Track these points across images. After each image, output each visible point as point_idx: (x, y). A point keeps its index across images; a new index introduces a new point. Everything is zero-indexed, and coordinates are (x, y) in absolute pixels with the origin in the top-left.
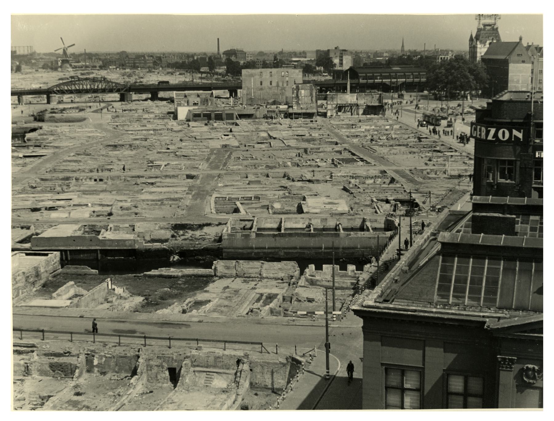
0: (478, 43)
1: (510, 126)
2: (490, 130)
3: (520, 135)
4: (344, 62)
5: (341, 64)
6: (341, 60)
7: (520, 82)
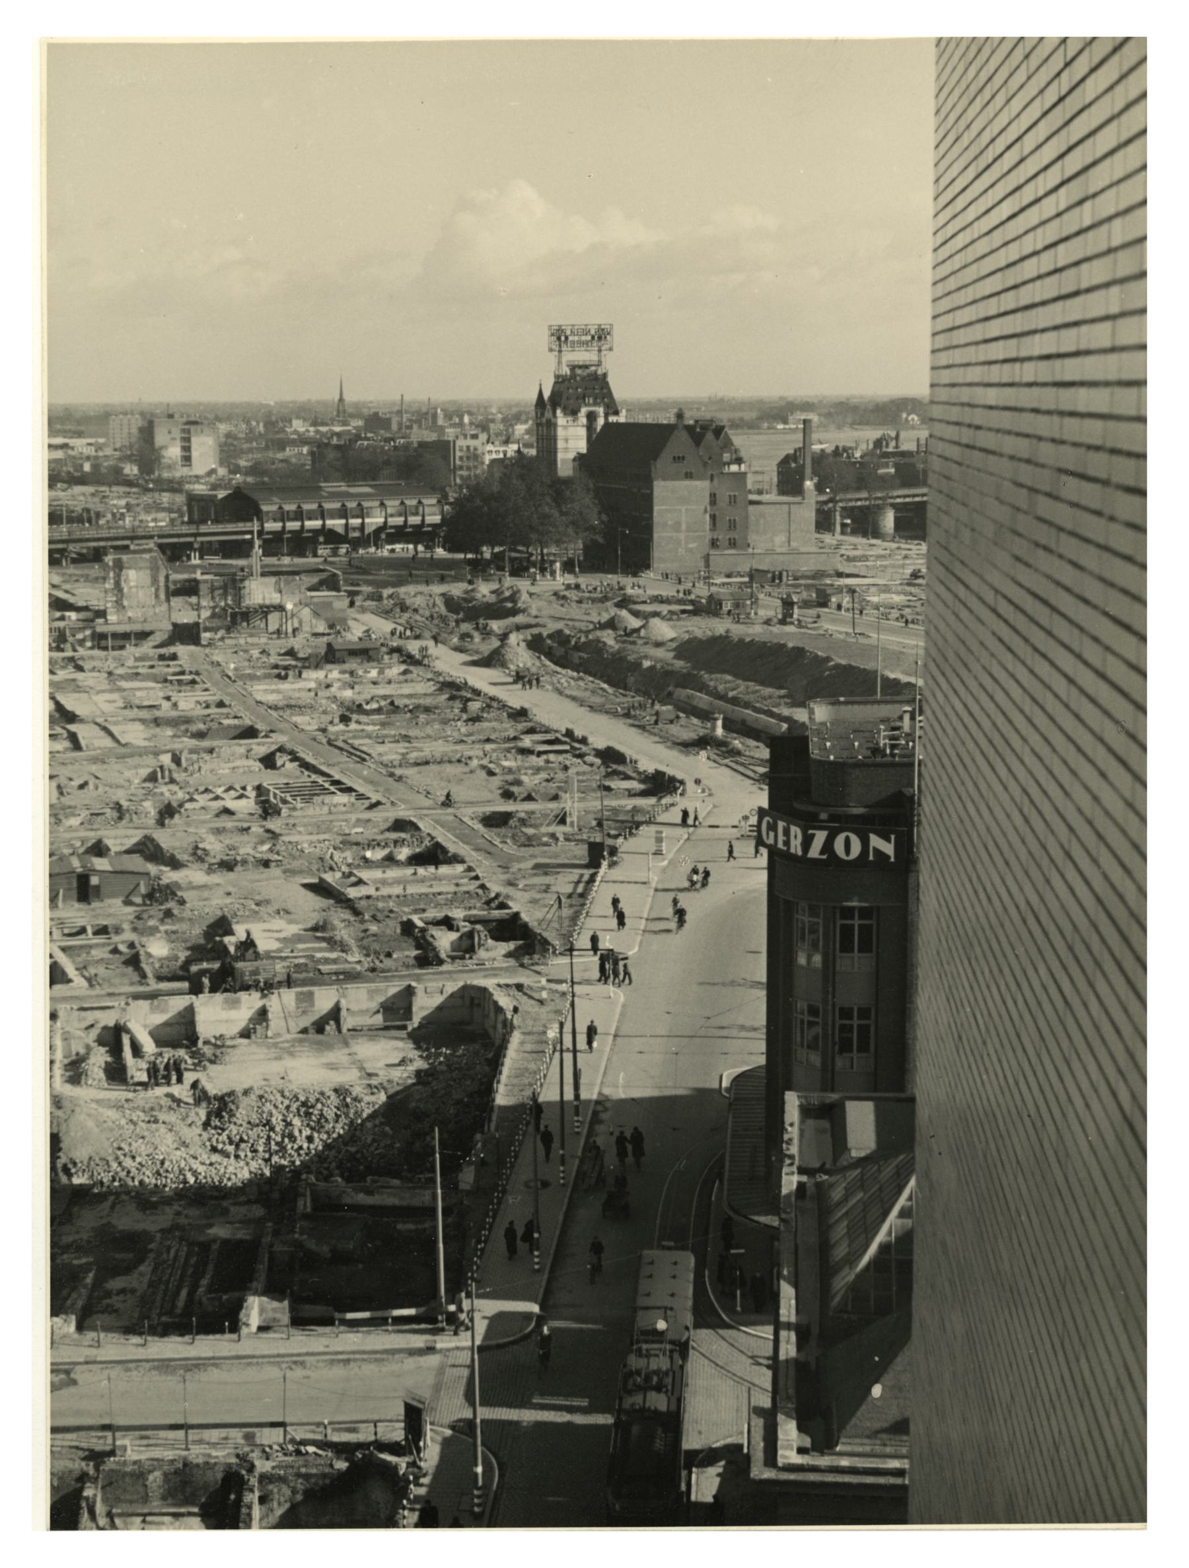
0: (559, 412)
1: (862, 826)
2: (813, 836)
3: (888, 848)
4: (195, 454)
5: (187, 459)
6: (187, 449)
7: (684, 527)
